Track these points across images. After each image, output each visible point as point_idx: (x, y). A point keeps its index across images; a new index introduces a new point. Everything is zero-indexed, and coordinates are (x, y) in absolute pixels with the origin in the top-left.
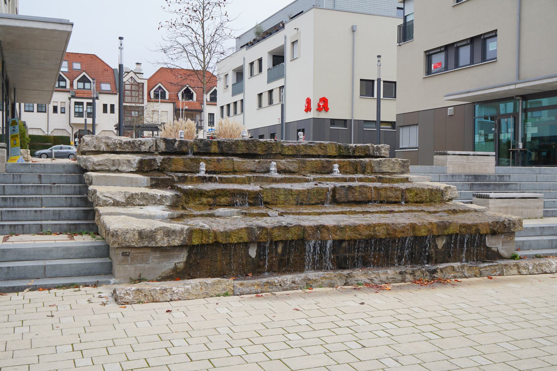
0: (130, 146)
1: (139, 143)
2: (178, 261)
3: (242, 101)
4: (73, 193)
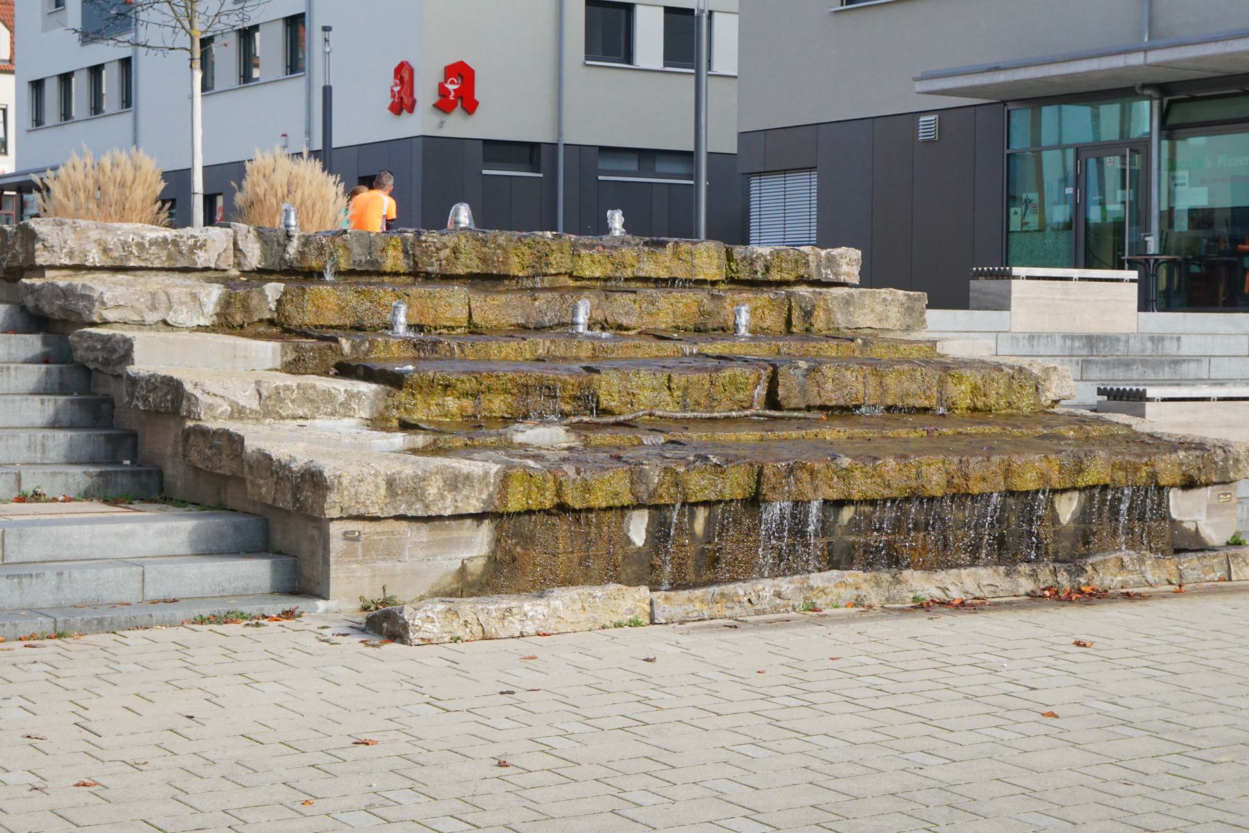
0: (165, 252)
1: (191, 242)
2: (468, 555)
3: (126, 63)
4: (44, 389)
